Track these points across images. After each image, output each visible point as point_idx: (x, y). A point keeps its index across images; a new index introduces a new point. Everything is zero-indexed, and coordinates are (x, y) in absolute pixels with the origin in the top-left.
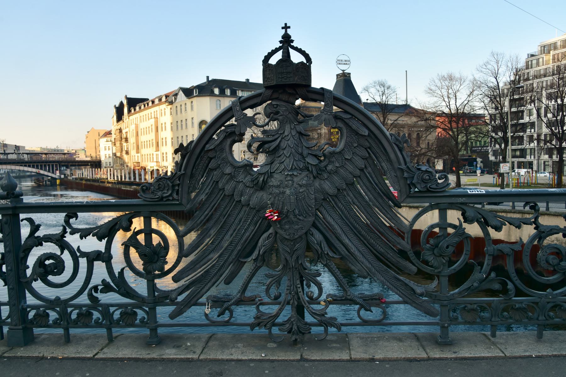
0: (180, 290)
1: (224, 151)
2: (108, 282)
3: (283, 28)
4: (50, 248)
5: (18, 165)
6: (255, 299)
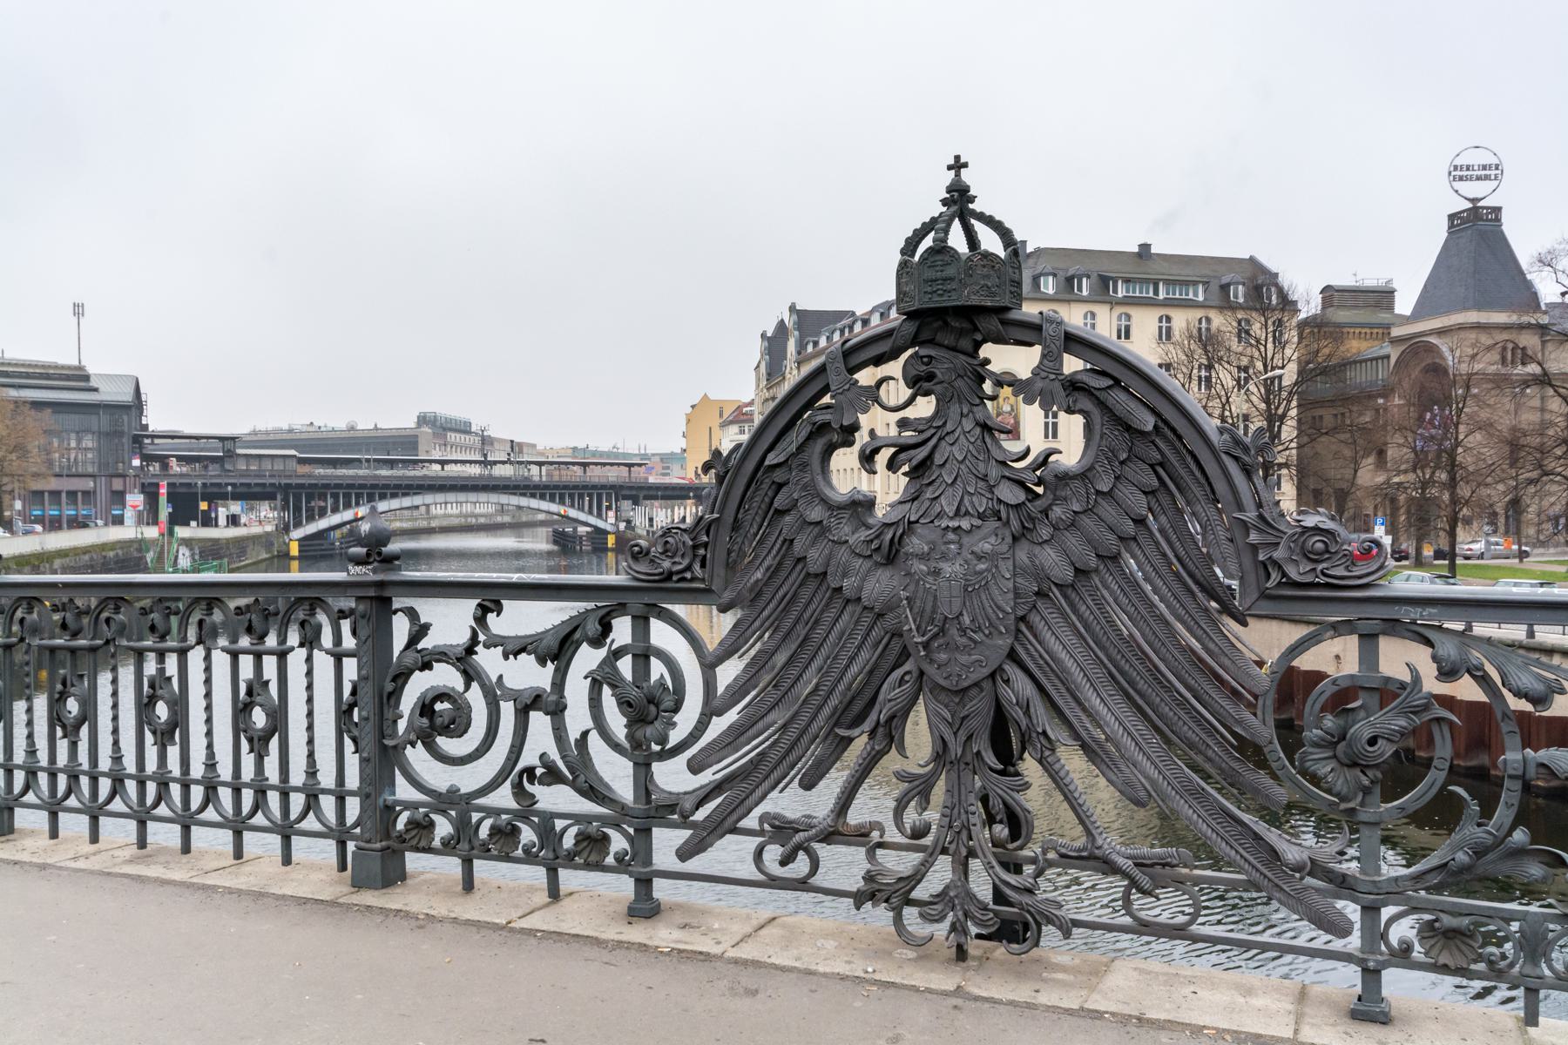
0: (702, 793)
1: (809, 468)
2: (553, 761)
3: (950, 168)
4: (445, 676)
5: (515, 494)
6: (870, 832)
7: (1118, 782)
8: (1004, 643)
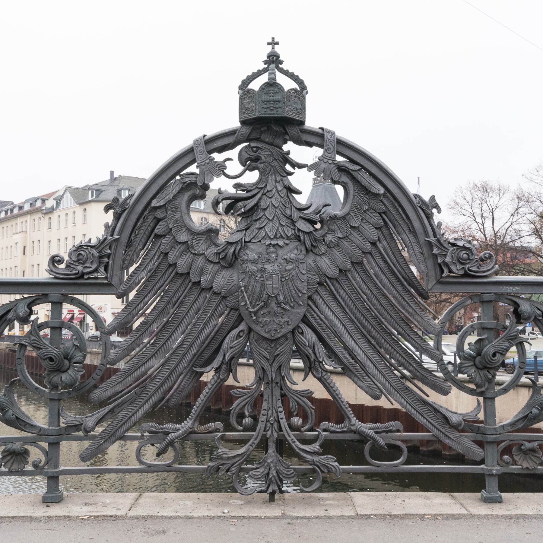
1: (179, 209)
3: (269, 44)
7: (365, 387)
8: (301, 311)
